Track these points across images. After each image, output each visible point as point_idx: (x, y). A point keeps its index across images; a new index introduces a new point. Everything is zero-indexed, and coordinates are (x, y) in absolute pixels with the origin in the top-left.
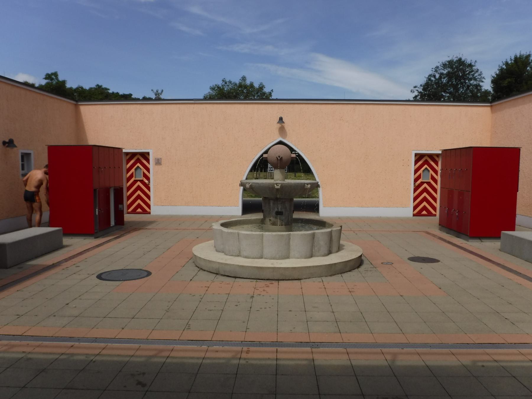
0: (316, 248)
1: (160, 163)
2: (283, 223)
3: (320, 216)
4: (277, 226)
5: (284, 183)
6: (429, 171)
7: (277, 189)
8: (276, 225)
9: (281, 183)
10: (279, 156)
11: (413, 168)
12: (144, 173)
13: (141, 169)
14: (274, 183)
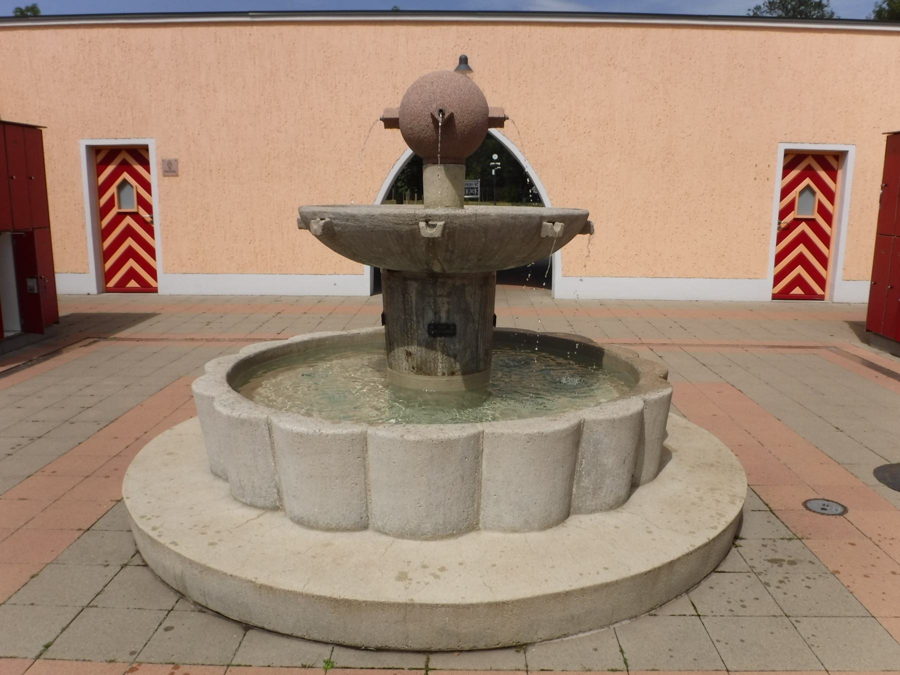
0: (586, 482)
1: (174, 172)
2: (458, 366)
3: (556, 297)
4: (436, 375)
5: (456, 217)
6: (814, 193)
7: (432, 242)
8: (429, 374)
9: (447, 217)
10: (441, 111)
11: (779, 184)
12: (139, 196)
13: (132, 186)
14: (415, 215)
